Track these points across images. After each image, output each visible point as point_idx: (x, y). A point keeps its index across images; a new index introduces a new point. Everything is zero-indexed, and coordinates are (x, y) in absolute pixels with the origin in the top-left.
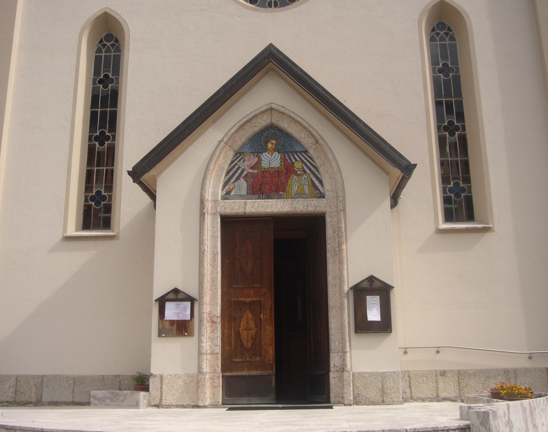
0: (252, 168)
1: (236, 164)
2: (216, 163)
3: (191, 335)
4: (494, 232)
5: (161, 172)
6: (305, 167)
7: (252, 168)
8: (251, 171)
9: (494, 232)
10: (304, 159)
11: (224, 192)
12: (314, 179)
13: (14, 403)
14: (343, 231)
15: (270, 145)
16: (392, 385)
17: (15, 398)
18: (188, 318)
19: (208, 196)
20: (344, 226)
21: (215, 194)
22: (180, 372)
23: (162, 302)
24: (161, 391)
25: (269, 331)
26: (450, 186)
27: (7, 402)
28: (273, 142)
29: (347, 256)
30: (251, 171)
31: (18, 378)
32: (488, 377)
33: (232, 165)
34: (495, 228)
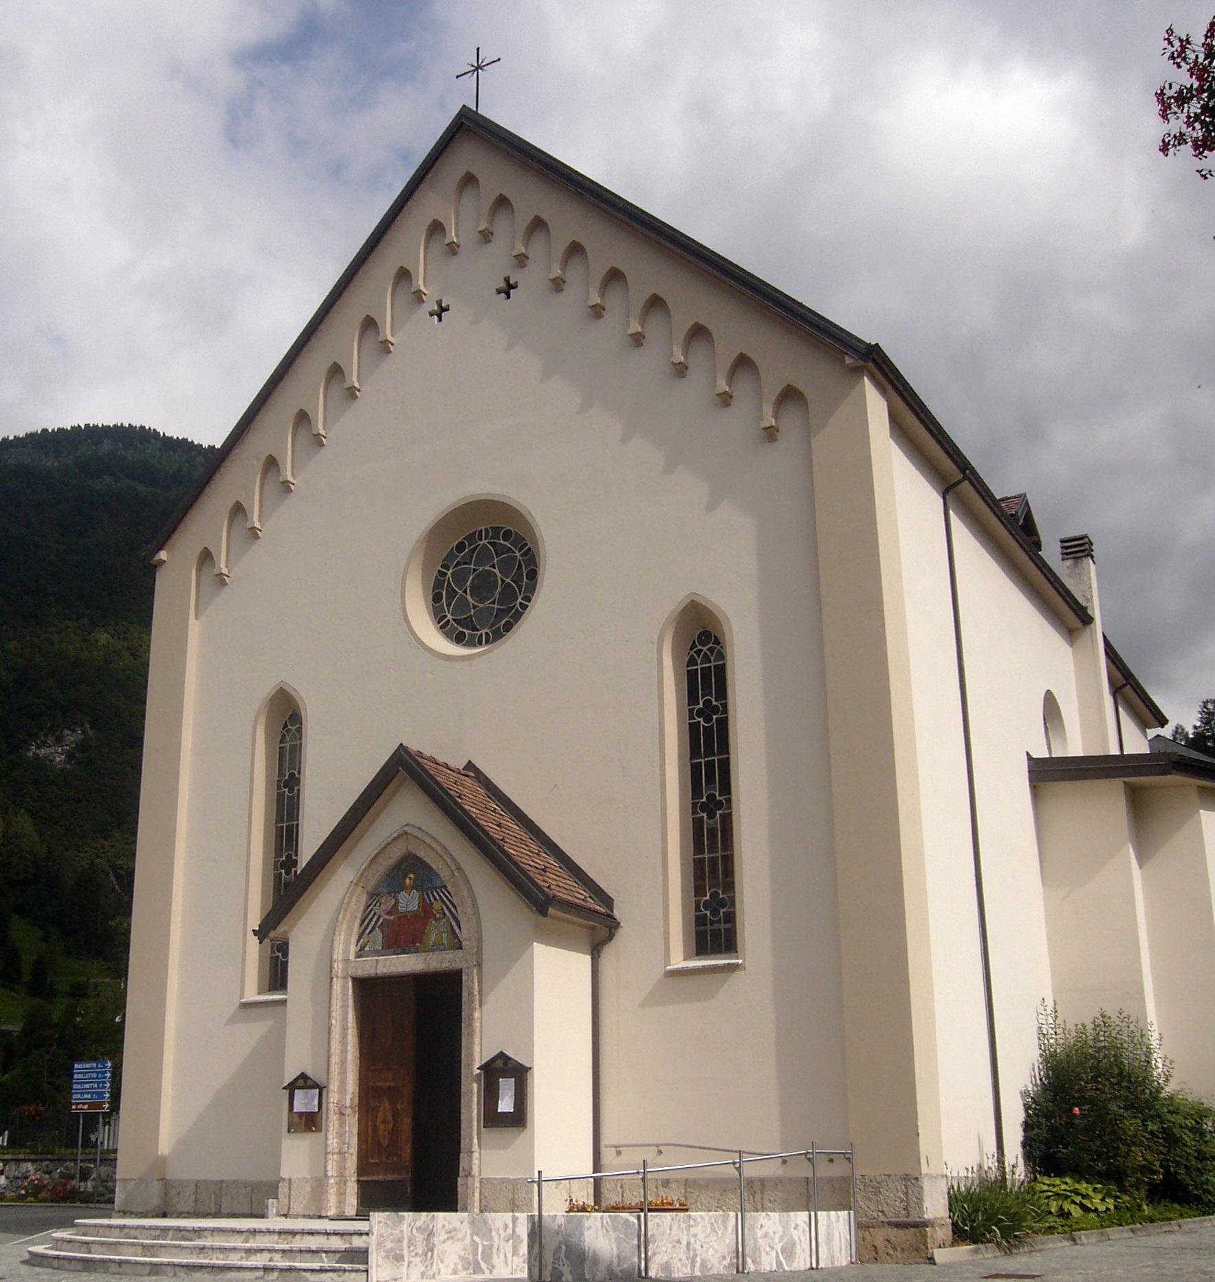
0: (389, 913)
1: (371, 910)
2: (345, 910)
3: (319, 1130)
4: (745, 970)
5: (292, 926)
6: (445, 908)
7: (389, 913)
8: (387, 917)
9: (745, 970)
10: (444, 897)
11: (359, 948)
12: (454, 923)
14: (476, 993)
15: (408, 881)
16: (524, 1195)
19: (338, 955)
20: (476, 987)
21: (346, 951)
22: (308, 1177)
23: (292, 1087)
24: (289, 1198)
25: (406, 1123)
26: (705, 898)
27: (188, 1213)
28: (412, 876)
29: (481, 1027)
30: (387, 917)
31: (197, 1184)
32: (725, 1191)
33: (367, 912)
34: (747, 965)
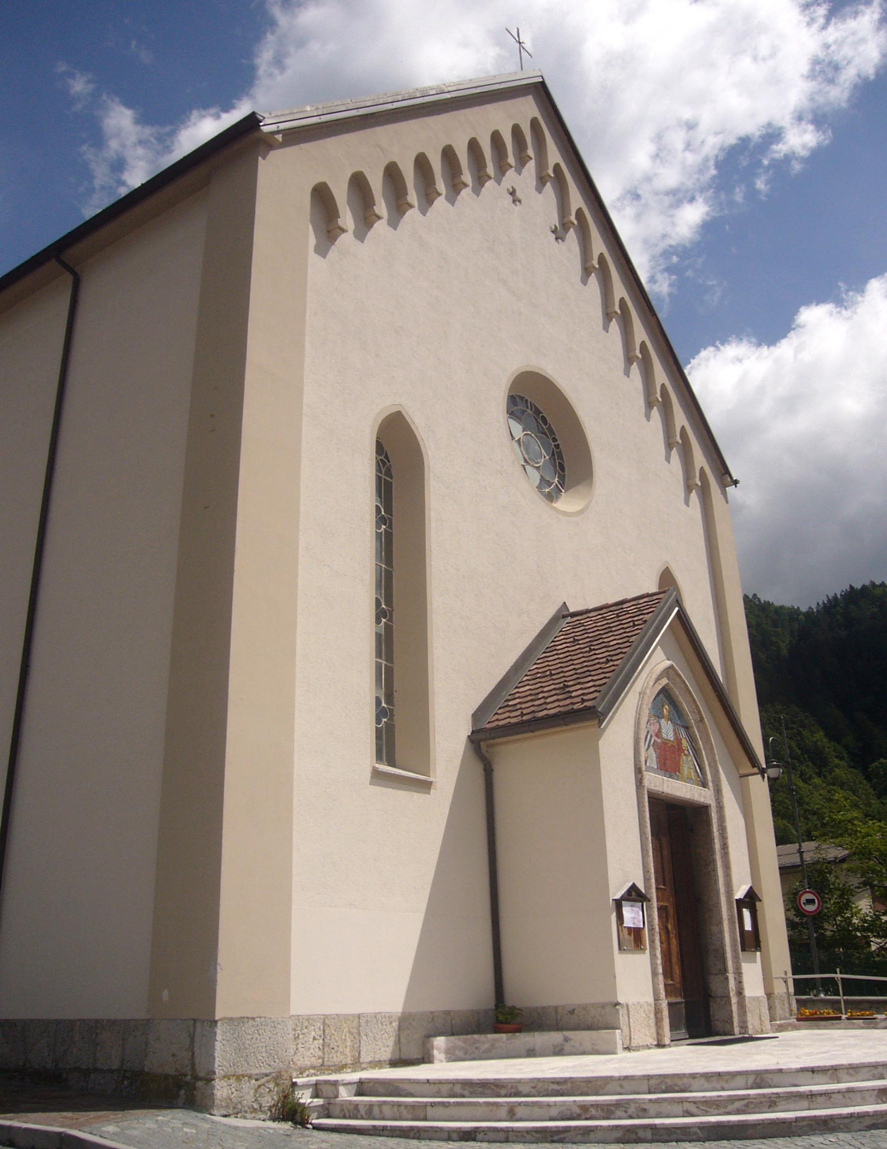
13: (323, 1068)
17: (323, 1059)
18: (642, 926)
23: (618, 904)
